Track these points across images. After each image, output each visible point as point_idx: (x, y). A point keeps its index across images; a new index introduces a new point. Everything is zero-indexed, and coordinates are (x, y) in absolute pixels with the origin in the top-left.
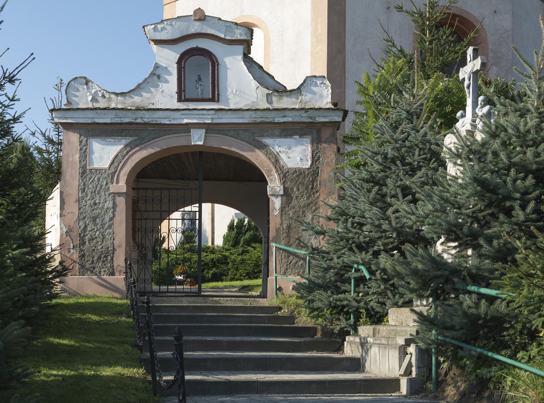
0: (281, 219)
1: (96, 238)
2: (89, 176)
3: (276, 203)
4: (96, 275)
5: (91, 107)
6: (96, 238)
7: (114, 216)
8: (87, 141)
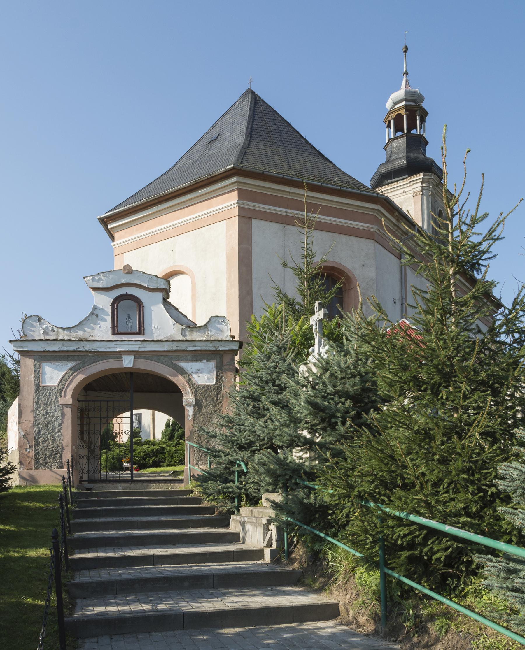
0: (194, 423)
1: (48, 439)
2: (42, 392)
3: (190, 411)
4: (48, 468)
5: (43, 339)
6: (48, 439)
7: (62, 422)
8: (40, 365)
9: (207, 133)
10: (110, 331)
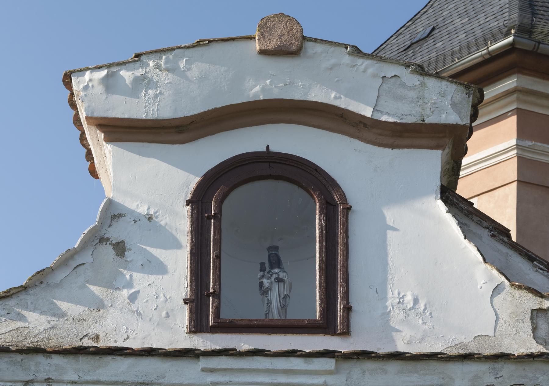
9: (398, 33)
10: (183, 316)
